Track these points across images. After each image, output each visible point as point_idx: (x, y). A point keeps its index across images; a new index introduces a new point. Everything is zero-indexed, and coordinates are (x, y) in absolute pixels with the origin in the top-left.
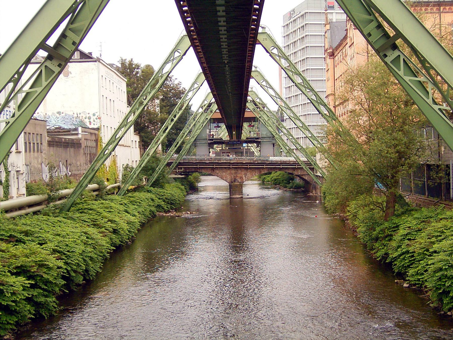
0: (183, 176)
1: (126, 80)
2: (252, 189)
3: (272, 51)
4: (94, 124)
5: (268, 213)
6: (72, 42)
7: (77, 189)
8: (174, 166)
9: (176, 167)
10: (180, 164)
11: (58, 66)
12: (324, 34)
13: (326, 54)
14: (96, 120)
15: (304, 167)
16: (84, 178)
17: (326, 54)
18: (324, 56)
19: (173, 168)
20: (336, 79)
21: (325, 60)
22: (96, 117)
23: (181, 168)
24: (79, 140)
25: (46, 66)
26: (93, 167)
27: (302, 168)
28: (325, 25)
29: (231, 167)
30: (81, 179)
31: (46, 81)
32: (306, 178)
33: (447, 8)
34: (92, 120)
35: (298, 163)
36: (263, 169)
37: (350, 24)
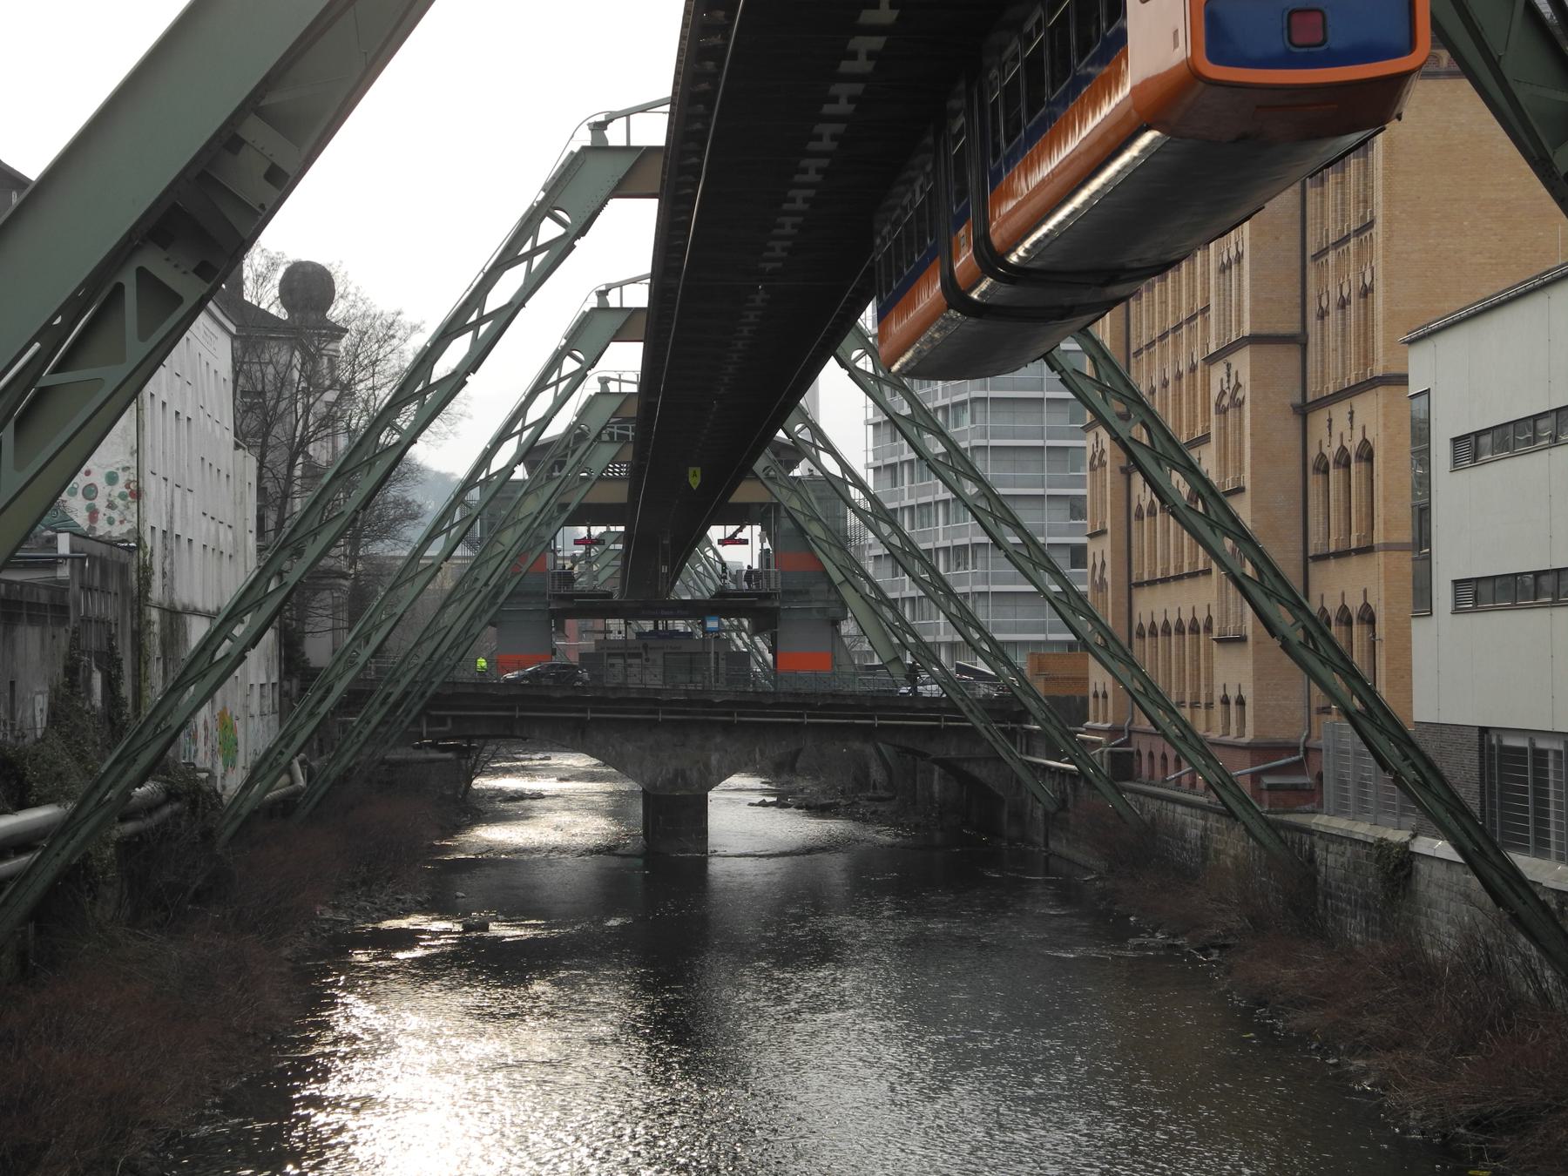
1: (233, 329)
2: (745, 821)
4: (111, 521)
5: (798, 929)
8: (414, 712)
9: (420, 714)
10: (438, 701)
11: (196, 271)
14: (119, 502)
15: (980, 726)
16: (116, 762)
20: (1139, 352)
22: (120, 487)
23: (441, 721)
24: (60, 588)
25: (142, 273)
27: (973, 728)
29: (660, 717)
30: (103, 769)
31: (143, 335)
32: (980, 772)
34: (101, 503)
36: (793, 735)
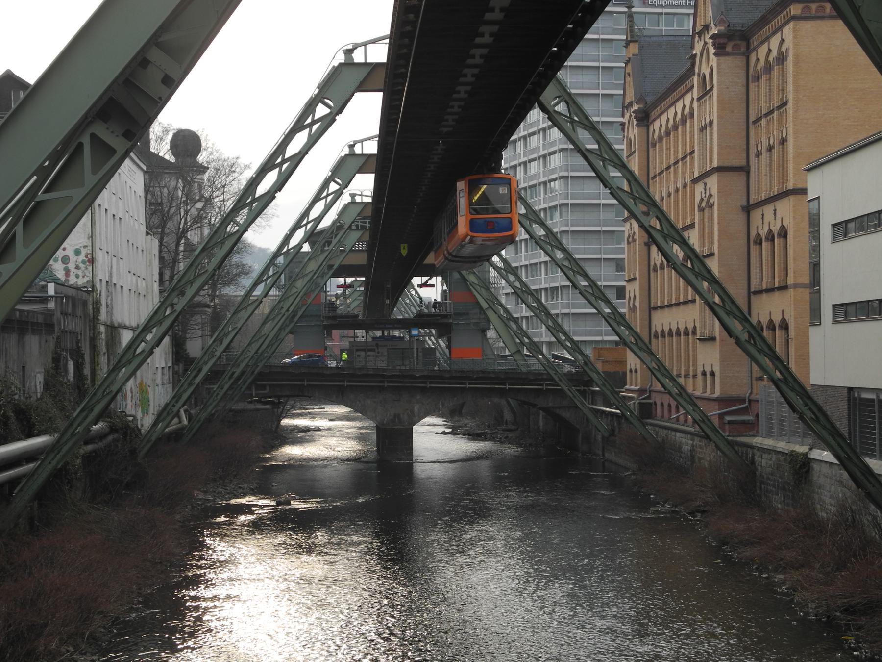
0: (267, 406)
1: (145, 168)
2: (434, 442)
3: (556, 109)
4: (77, 276)
6: (162, 76)
7: (64, 439)
8: (249, 381)
9: (251, 384)
11: (123, 135)
12: (623, 65)
13: (627, 116)
14: (82, 265)
15: (566, 389)
16: (81, 411)
17: (627, 116)
18: (621, 119)
19: (244, 387)
21: (623, 130)
22: (82, 257)
23: (263, 387)
24: (49, 314)
26: (106, 385)
27: (562, 390)
28: (627, 43)
29: (306, 383)
31: (94, 172)
32: (566, 415)
33: (814, 6)
34: (72, 266)
35: (553, 380)
36: (461, 394)
37: (702, 43)
